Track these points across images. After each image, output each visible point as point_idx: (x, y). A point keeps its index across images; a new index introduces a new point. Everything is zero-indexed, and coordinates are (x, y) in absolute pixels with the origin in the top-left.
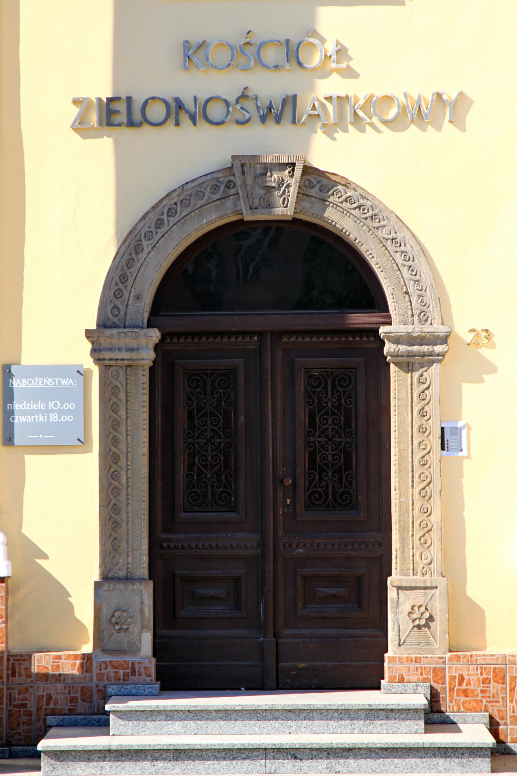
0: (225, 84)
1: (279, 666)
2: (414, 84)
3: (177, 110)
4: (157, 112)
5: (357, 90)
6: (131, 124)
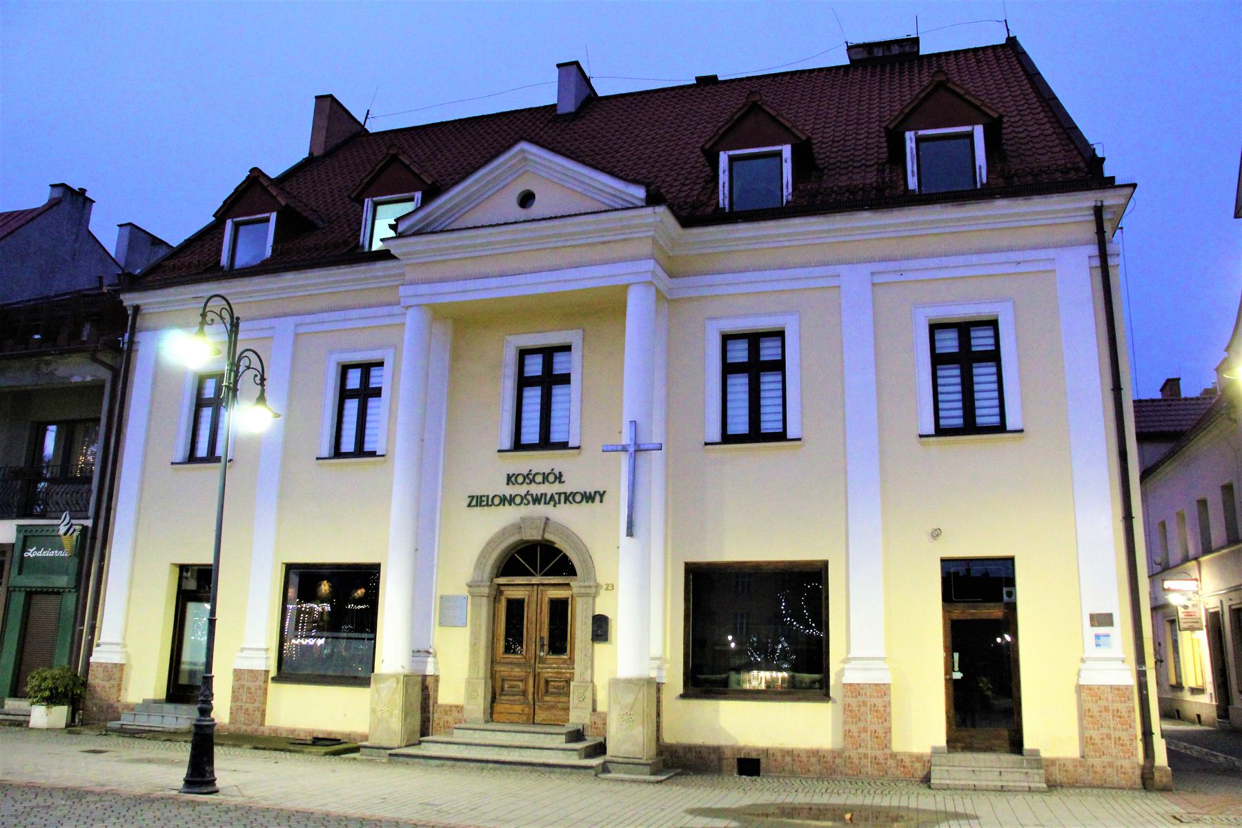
0: (522, 490)
1: (92, 660)
2: (590, 489)
3: (511, 500)
4: (497, 501)
5: (567, 488)
6: (487, 505)
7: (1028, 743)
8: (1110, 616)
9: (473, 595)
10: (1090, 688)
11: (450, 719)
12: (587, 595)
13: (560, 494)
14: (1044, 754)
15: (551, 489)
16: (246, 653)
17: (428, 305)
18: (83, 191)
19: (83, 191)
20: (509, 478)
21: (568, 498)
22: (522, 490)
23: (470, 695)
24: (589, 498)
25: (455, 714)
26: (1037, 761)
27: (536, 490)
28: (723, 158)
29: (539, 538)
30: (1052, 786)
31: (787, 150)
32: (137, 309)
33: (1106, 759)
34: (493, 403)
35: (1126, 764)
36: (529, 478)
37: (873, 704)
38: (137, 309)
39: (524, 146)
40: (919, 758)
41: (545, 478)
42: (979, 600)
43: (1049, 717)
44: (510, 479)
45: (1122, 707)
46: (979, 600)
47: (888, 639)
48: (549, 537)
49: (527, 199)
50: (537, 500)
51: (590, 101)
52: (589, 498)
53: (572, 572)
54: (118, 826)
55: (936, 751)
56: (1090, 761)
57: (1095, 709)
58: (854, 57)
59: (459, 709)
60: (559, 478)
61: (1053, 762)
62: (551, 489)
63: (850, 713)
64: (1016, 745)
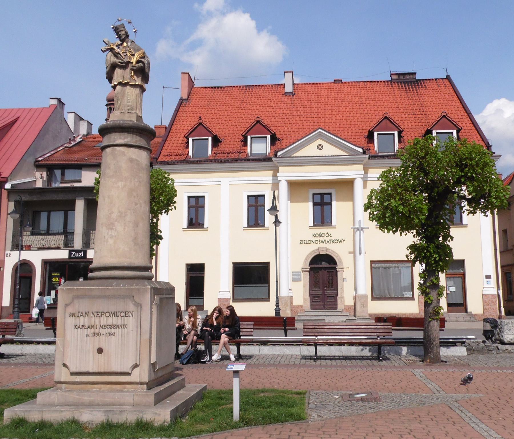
0: (318, 239)
2: (340, 239)
5: (333, 238)
7: (469, 310)
8: (490, 276)
10: (486, 295)
11: (299, 310)
12: (341, 271)
13: (330, 240)
14: (473, 313)
15: (329, 238)
16: (221, 293)
17: (286, 180)
18: (161, 238)
19: (161, 238)
23: (305, 302)
24: (340, 242)
25: (300, 308)
26: (471, 315)
33: (490, 313)
34: (307, 209)
35: (495, 314)
36: (320, 235)
44: (360, 221)
45: (494, 300)
48: (327, 253)
50: (323, 242)
54: (513, 355)
56: (486, 314)
57: (487, 300)
58: (393, 78)
59: (302, 306)
61: (476, 315)
64: (466, 312)
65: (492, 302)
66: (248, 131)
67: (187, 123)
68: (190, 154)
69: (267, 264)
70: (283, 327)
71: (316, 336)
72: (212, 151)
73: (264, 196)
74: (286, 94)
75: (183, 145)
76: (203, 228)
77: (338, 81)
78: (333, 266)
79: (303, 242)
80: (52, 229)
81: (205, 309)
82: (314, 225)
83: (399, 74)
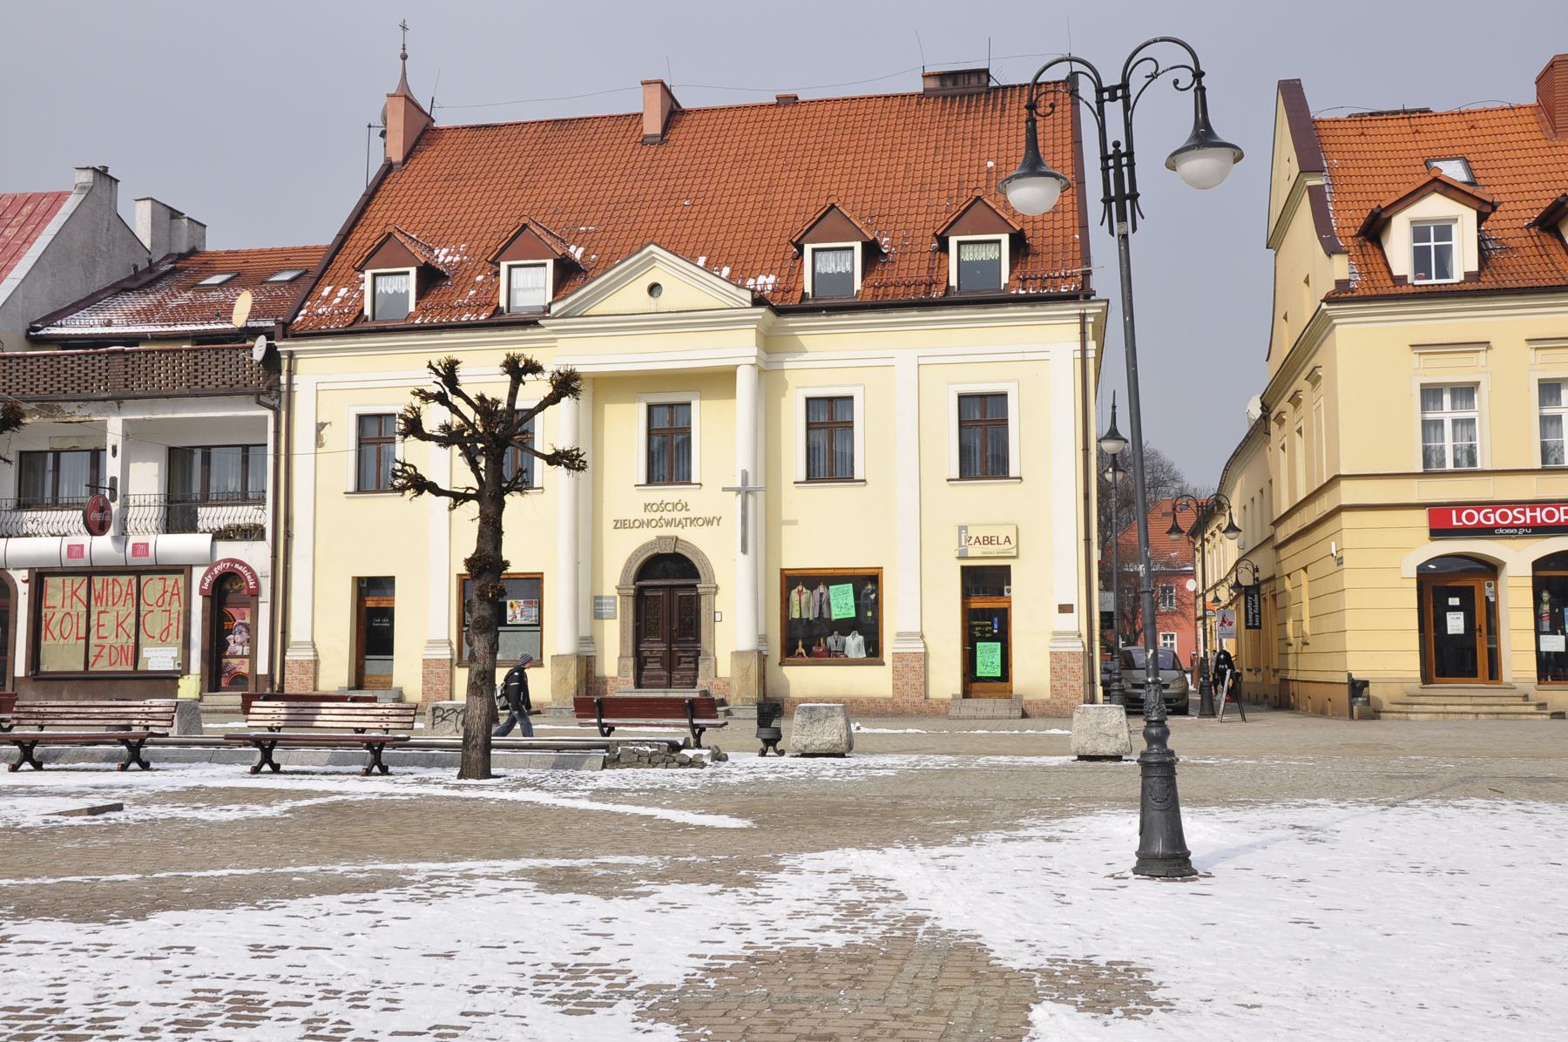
0: (657, 516)
2: (710, 515)
9: (622, 595)
20: (646, 506)
21: (693, 521)
22: (657, 516)
24: (709, 522)
27: (667, 516)
28: (808, 248)
29: (785, 517)
30: (1025, 715)
31: (858, 246)
32: (291, 354)
36: (662, 506)
37: (917, 666)
38: (291, 354)
39: (652, 248)
40: (942, 701)
41: (675, 506)
42: (985, 595)
43: (1032, 670)
46: (985, 595)
47: (921, 614)
49: (654, 289)
50: (668, 524)
51: (674, 114)
52: (709, 522)
53: (697, 576)
55: (955, 697)
60: (685, 507)
62: (678, 515)
63: (897, 674)
65: (1072, 670)
66: (503, 250)
67: (365, 237)
68: (953, 282)
69: (963, 568)
70: (687, 721)
71: (42, 727)
72: (1011, 272)
73: (849, 399)
74: (645, 141)
75: (927, 255)
76: (690, 483)
77: (962, 88)
78: (691, 582)
79: (621, 524)
80: (65, 492)
81: (396, 683)
82: (650, 481)
83: (942, 76)
